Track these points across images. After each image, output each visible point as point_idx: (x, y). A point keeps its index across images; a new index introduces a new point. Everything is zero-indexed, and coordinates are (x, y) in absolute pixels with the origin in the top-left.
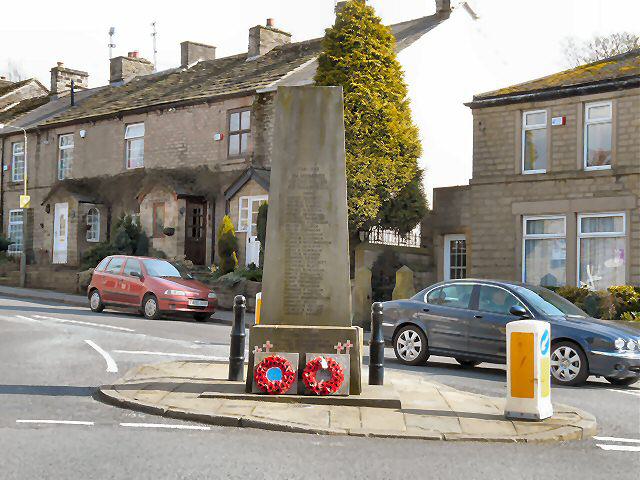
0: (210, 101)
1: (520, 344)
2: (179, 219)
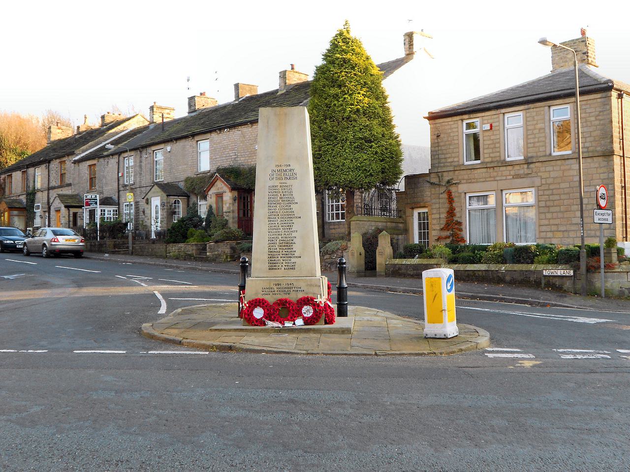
1: (432, 285)
2: (233, 204)
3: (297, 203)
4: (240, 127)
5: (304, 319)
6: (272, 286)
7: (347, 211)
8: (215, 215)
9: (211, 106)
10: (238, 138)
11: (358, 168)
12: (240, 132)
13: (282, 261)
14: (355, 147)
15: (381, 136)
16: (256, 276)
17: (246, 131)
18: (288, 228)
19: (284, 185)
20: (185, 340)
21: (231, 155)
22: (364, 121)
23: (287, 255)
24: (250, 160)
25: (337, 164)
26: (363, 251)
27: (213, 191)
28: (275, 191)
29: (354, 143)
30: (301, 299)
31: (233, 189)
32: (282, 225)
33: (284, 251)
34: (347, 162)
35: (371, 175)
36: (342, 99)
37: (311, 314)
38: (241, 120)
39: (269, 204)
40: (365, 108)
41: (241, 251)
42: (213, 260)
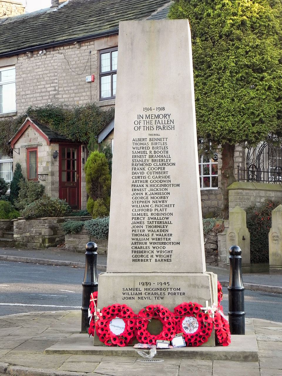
0: (81, 41)
2: (53, 163)
3: (174, 164)
4: (62, 48)
5: (185, 336)
6: (137, 286)
7: (224, 176)
8: (24, 180)
9: (16, 15)
10: (59, 64)
11: (242, 111)
12: (62, 56)
13: (151, 249)
14: (237, 80)
15: (277, 62)
16: (114, 269)
17: (71, 55)
18: (160, 200)
19: (156, 137)
20: (12, 368)
21: (49, 89)
22: (251, 38)
23: (159, 239)
24: (78, 99)
25: (211, 105)
26: (247, 234)
27: (22, 143)
28: (142, 146)
29: (236, 73)
30: (180, 306)
31: (52, 141)
32: (152, 196)
33: (155, 233)
34: (226, 103)
35: (261, 121)
36: (220, 6)
37: (195, 330)
38: (64, 38)
39: (133, 165)
40: (254, 19)
41: (66, 232)
42: (23, 245)
